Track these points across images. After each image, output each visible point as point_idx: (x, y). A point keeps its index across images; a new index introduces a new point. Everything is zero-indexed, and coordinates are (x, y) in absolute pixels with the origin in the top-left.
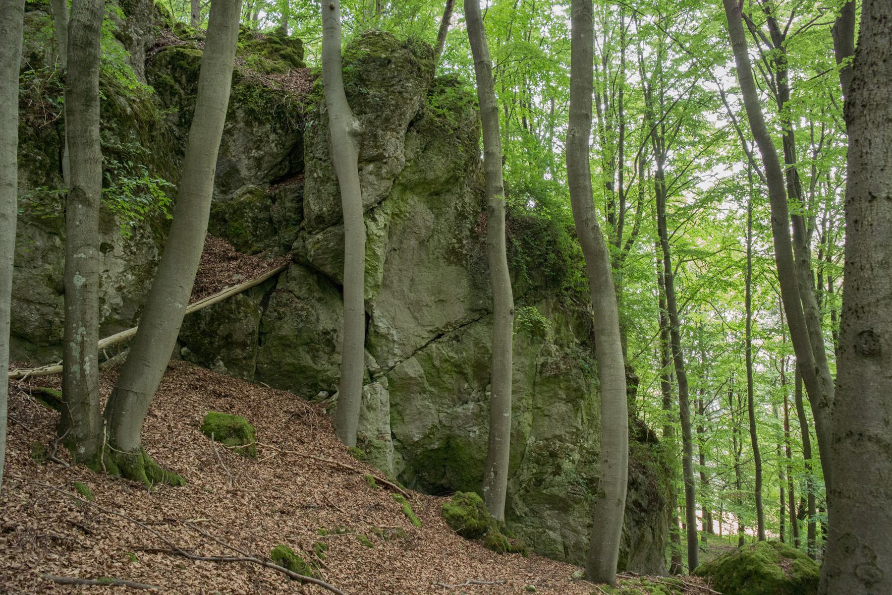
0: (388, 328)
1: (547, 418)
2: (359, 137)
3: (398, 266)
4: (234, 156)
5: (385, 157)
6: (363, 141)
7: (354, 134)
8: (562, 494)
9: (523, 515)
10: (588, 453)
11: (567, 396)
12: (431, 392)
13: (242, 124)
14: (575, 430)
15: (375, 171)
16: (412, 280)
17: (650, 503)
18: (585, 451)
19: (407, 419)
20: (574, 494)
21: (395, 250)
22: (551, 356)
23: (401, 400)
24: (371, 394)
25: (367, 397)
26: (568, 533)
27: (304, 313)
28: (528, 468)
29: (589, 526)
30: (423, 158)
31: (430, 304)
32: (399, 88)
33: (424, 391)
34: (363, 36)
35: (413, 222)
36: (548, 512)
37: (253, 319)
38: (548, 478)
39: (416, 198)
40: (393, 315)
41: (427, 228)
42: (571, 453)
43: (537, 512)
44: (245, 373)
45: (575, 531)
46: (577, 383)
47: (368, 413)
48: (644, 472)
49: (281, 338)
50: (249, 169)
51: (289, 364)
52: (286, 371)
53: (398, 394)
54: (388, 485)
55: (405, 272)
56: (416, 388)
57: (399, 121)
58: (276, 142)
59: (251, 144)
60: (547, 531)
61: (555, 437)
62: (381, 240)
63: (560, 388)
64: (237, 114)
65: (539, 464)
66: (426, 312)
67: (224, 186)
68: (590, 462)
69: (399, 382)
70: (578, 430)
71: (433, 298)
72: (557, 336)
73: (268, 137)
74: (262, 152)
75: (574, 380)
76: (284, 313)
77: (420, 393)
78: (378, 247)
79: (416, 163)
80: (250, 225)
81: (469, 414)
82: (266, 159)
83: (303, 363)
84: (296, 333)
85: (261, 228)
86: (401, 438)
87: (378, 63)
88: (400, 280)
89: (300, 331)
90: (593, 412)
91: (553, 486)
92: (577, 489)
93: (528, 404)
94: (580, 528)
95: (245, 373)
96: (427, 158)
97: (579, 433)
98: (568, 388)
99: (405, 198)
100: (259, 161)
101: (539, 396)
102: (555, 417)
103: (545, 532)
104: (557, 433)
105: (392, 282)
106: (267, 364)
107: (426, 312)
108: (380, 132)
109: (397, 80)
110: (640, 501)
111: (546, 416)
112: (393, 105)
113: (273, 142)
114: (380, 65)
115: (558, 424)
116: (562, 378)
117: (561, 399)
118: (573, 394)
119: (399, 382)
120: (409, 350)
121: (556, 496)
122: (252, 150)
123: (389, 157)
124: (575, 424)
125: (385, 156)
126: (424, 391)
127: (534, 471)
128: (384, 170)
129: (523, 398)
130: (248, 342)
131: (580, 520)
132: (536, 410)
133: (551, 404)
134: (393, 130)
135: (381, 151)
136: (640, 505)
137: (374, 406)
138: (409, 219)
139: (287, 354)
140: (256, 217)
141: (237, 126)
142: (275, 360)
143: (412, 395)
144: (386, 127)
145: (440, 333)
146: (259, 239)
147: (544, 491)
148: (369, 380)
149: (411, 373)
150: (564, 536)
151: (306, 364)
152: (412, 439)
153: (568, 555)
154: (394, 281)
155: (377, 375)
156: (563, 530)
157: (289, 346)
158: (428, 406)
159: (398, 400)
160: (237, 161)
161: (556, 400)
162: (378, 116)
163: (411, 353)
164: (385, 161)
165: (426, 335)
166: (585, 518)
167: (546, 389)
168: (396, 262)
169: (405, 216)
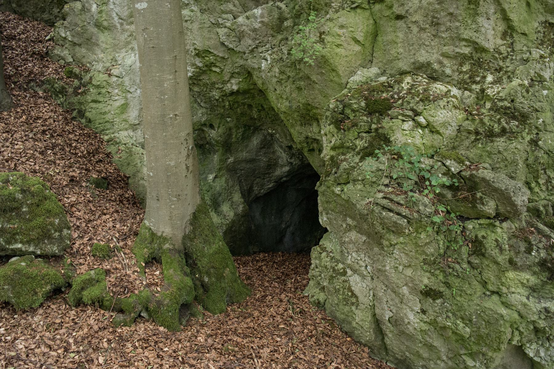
14: (467, 51)
18: (488, 105)
20: (384, 208)
25: (89, 10)
60: (349, 272)
65: (339, 129)
68: (491, 135)
70: (479, 49)
81: (257, 25)
92: (400, 199)
94: (405, 290)
102: (417, 17)
103: (344, 273)
104: (423, 57)
111: (399, 17)
115: (424, 35)
137: (105, 24)
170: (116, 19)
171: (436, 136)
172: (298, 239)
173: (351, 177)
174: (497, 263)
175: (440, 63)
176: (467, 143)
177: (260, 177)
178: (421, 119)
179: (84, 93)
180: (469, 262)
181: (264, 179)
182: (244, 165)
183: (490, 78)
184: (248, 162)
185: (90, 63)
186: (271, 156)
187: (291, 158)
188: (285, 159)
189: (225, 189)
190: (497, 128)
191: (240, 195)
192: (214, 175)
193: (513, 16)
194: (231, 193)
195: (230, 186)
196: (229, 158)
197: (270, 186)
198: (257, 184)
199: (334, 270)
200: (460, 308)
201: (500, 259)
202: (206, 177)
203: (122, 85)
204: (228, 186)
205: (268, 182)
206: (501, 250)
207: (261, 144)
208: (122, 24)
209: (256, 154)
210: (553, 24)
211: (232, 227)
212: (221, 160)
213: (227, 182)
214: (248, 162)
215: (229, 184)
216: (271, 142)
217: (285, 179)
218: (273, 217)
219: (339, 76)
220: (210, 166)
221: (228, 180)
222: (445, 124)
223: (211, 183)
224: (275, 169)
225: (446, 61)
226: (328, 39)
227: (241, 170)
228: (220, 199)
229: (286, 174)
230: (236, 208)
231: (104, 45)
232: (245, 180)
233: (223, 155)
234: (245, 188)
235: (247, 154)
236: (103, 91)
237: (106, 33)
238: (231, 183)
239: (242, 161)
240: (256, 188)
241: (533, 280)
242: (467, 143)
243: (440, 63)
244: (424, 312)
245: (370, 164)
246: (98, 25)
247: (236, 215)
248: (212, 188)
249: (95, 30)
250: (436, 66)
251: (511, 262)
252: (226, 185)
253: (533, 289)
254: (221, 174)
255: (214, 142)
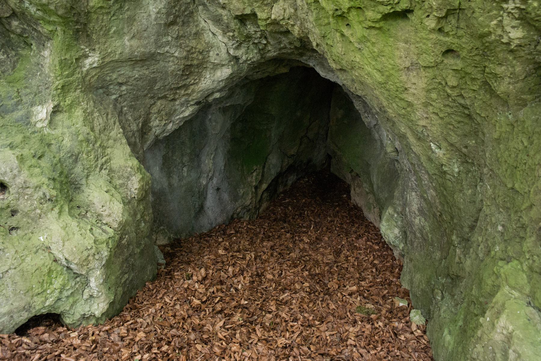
172: (226, 196)
177: (165, 97)
181: (174, 100)
182: (126, 71)
184: (137, 62)
186: (193, 43)
187: (237, 48)
188: (224, 51)
189: (88, 141)
191: (128, 149)
192: (50, 106)
194: (103, 147)
195: (97, 129)
196: (87, 57)
197: (187, 114)
198: (159, 112)
202: (28, 116)
204: (92, 129)
205: (182, 105)
207: (168, 14)
209: (156, 41)
210: (170, 7)
211: (121, 238)
212: (63, 64)
213: (88, 119)
214: (137, 62)
215: (96, 123)
216: (192, 7)
217: (217, 95)
218: (185, 169)
220: (34, 82)
221: (92, 113)
223: (46, 131)
224: (200, 75)
227: (121, 84)
228: (78, 169)
229: (222, 84)
230: (121, 185)
232: (131, 107)
233: (69, 48)
234: (134, 127)
235: (135, 43)
238: (99, 122)
239: (121, 62)
240: (157, 122)
247: (126, 202)
248: (49, 145)
252: (87, 130)
254: (68, 102)
255: (33, 10)
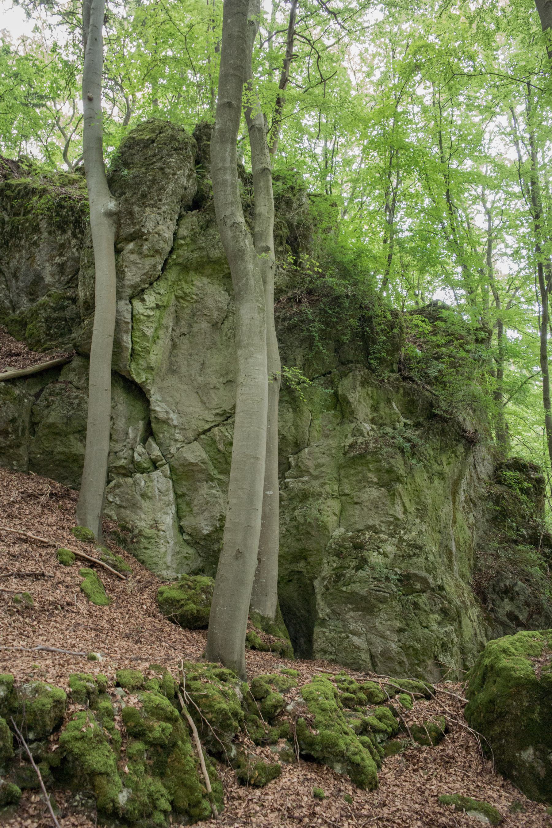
0: (167, 412)
1: (357, 506)
2: (114, 217)
3: (187, 350)
4: (39, 265)
5: (143, 234)
6: (119, 220)
7: (109, 214)
8: (364, 592)
9: (327, 618)
10: (409, 545)
11: (379, 479)
12: (219, 480)
13: (45, 235)
14: (392, 519)
15: (136, 249)
16: (203, 364)
17: (530, 616)
18: (404, 544)
19: (195, 510)
20: (377, 591)
21: (185, 335)
22: (363, 436)
23: (189, 490)
24: (146, 482)
25: (139, 485)
26: (374, 638)
27: (77, 401)
28: (328, 562)
29: (401, 631)
30: (203, 235)
31: (218, 386)
32: (159, 164)
33: (210, 478)
34: (138, 125)
35: (203, 304)
36: (352, 614)
37: (12, 406)
38: (349, 573)
39: (205, 280)
40: (177, 400)
41: (220, 309)
42: (380, 545)
43: (339, 615)
44: (14, 463)
45: (382, 637)
46: (389, 463)
47: (143, 502)
48: (527, 580)
49: (51, 426)
50: (53, 275)
51: (60, 453)
52: (59, 460)
53: (184, 483)
54: (95, 562)
55: (196, 357)
56: (200, 476)
57: (158, 196)
58: (77, 247)
59: (55, 252)
61: (369, 528)
62: (151, 319)
63: (370, 470)
64: (41, 226)
65: (340, 558)
66: (213, 395)
67: (32, 294)
68: (410, 556)
69: (181, 470)
70: (397, 519)
71: (221, 380)
72: (375, 415)
73: (70, 243)
74: (65, 258)
75: (385, 460)
76: (53, 401)
77: (207, 482)
78: (148, 327)
79: (194, 241)
80: (44, 324)
82: (69, 264)
83: (74, 451)
84: (65, 421)
85: (55, 328)
86: (190, 531)
87: (142, 145)
88: (189, 365)
89: (69, 418)
90: (423, 500)
91: (354, 582)
92: (382, 586)
93: (333, 490)
94: (388, 633)
95: (14, 463)
96: (209, 235)
97: (399, 522)
98: (378, 470)
99: (189, 279)
100: (62, 267)
101: (345, 480)
102: (366, 504)
103: (348, 637)
104: (371, 522)
105: (180, 367)
106: (40, 454)
107: (213, 395)
108: (136, 209)
109: (159, 157)
110: (517, 613)
111: (356, 503)
112: (149, 181)
113: (74, 247)
114: (144, 147)
115: (371, 512)
116: (369, 457)
117: (372, 482)
118: (386, 477)
119: (181, 470)
120: (191, 435)
121: (356, 593)
122: (55, 257)
123: (149, 233)
124: (391, 512)
125: (143, 232)
126: (210, 478)
127: (335, 565)
128: (145, 247)
129: (325, 484)
130: (10, 430)
131: (389, 623)
132: (344, 498)
133: (360, 489)
134: (153, 206)
135: (138, 227)
136: (516, 618)
137: (150, 494)
138: (196, 301)
139: (58, 443)
140: (49, 317)
141: (42, 237)
142: (47, 449)
143: (198, 484)
144: (143, 203)
145: (228, 415)
146: (51, 337)
147: (344, 589)
148: (152, 468)
149: (191, 458)
150: (370, 643)
151: (77, 452)
152: (201, 532)
153: (377, 665)
154: (182, 366)
155: (159, 463)
156: (369, 635)
157: (59, 434)
158: (215, 494)
159: (184, 490)
160: (42, 269)
161: (366, 484)
162: (135, 193)
163: (193, 438)
164: (144, 237)
165: (210, 418)
166: (395, 621)
167: (352, 472)
168: (184, 345)
169: (192, 298)
170: (157, 491)
171: (387, 559)
173: (352, 580)
174: (425, 611)
175: (380, 525)
176: (399, 561)
178: (381, 550)
179: (138, 542)
180: (414, 613)
183: (402, 532)
185: (133, 521)
190: (411, 553)
193: (406, 505)
199: (340, 637)
200: (415, 635)
201: (426, 609)
203: (165, 537)
206: (426, 605)
208: (160, 496)
219: (329, 532)
222: (390, 553)
225: (382, 524)
226: (323, 513)
231: (146, 509)
236: (153, 541)
237: (148, 501)
241: (439, 618)
242: (399, 561)
243: (380, 525)
244: (399, 641)
245: (360, 573)
246: (144, 496)
249: (139, 498)
250: (378, 527)
251: (431, 610)
253: (439, 623)
